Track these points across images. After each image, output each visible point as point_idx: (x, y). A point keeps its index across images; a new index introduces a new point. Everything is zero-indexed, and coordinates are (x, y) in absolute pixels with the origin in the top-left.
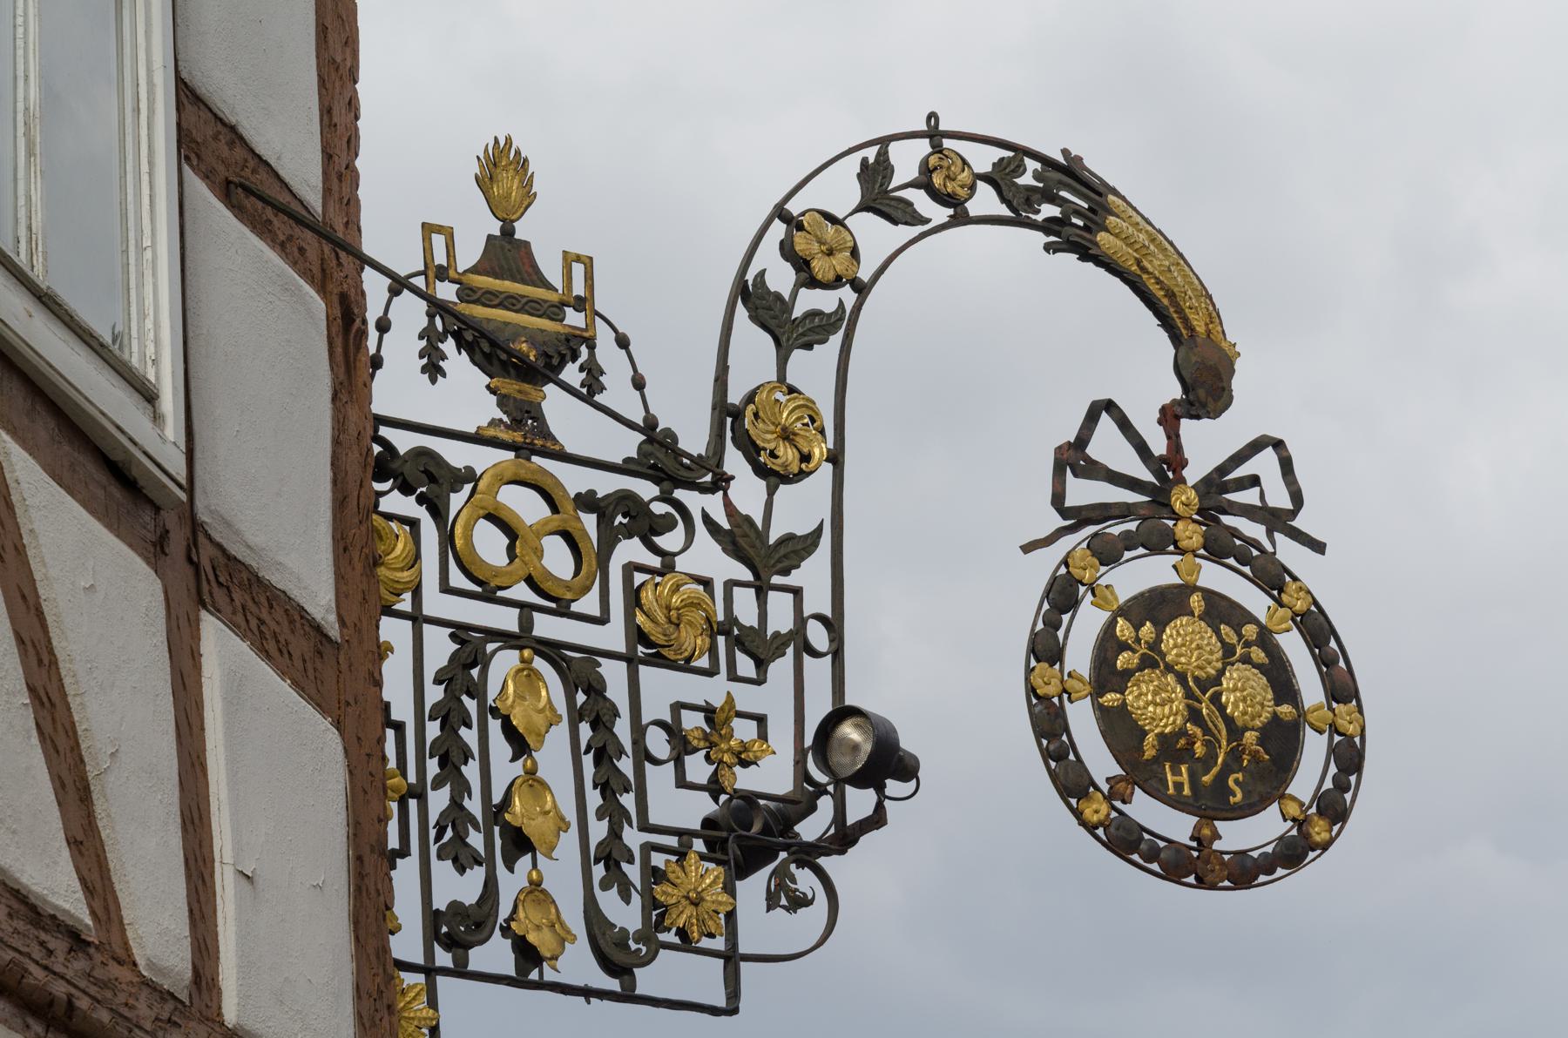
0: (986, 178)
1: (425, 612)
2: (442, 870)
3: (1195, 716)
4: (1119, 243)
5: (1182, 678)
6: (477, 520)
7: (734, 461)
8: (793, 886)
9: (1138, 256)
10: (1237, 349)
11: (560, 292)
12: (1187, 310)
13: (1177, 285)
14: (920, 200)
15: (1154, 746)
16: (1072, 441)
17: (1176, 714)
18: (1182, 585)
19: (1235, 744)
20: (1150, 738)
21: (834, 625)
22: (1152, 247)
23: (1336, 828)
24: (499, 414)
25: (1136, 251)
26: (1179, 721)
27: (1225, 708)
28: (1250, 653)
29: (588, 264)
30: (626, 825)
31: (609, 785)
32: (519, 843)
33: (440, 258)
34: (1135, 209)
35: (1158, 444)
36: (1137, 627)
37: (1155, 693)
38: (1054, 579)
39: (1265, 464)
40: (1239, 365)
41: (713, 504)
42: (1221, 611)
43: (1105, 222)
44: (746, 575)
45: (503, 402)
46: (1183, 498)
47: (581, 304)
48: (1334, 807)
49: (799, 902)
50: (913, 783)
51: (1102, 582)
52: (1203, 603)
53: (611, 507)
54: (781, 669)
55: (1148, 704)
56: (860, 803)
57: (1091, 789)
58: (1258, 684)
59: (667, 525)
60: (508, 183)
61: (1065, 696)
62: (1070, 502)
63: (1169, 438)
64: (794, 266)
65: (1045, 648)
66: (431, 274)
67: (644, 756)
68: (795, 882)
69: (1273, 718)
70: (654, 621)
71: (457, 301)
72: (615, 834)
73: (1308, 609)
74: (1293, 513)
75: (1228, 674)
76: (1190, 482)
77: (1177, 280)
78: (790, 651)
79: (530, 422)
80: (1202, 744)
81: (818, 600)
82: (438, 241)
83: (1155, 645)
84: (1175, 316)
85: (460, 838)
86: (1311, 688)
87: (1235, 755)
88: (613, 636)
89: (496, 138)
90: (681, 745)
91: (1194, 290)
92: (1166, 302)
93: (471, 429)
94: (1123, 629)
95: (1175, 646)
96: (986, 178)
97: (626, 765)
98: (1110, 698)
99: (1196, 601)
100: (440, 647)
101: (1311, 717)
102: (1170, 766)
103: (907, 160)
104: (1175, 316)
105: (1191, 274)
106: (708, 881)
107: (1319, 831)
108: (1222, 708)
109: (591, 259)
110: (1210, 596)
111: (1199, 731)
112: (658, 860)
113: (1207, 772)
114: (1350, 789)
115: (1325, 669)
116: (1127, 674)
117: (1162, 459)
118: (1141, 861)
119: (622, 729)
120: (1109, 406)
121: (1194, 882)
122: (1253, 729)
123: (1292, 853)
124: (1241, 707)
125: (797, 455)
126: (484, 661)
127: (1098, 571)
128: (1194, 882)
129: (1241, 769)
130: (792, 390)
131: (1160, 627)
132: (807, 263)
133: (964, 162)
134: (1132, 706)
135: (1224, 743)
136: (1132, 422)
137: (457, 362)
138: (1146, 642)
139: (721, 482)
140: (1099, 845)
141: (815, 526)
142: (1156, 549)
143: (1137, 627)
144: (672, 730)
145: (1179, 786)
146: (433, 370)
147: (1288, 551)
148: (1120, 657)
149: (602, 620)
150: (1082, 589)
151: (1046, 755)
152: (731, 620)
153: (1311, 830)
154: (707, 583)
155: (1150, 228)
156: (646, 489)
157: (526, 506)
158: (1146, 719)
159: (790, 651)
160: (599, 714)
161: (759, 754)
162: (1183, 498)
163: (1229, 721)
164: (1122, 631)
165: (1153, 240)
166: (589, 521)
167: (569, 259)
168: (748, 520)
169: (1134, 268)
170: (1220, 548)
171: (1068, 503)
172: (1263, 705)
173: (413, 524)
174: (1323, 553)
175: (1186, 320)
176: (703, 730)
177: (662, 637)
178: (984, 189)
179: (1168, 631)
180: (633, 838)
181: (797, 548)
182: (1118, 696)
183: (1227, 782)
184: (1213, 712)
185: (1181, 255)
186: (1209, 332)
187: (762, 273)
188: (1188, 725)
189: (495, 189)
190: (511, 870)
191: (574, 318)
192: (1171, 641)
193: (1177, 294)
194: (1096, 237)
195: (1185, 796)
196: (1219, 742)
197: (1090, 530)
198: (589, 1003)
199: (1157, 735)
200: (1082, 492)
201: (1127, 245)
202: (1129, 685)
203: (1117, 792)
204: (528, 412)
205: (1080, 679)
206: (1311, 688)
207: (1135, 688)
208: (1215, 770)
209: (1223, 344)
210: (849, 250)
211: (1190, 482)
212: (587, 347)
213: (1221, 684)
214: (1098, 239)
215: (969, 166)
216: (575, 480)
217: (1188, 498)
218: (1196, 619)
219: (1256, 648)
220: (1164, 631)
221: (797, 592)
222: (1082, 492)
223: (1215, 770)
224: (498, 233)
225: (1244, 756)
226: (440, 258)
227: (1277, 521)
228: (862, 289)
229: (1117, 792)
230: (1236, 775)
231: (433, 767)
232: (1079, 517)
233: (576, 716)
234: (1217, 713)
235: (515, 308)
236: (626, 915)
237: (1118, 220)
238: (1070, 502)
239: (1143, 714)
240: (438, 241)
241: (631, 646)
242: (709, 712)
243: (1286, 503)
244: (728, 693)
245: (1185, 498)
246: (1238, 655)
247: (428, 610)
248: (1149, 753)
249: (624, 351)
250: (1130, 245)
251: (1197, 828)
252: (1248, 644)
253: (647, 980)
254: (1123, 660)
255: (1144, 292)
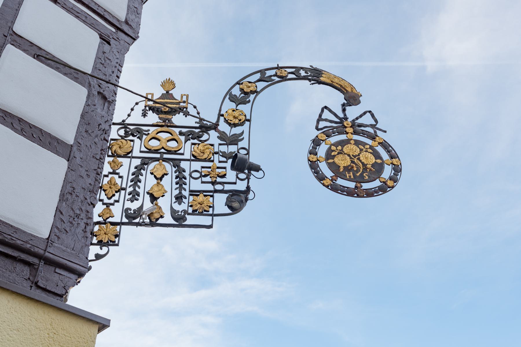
3: (353, 162)
5: (349, 155)
18: (348, 139)
19: (364, 167)
57: (326, 178)
77: (342, 83)
83: (342, 150)
86: (385, 156)
89: (167, 79)
92: (340, 87)
98: (331, 161)
101: (386, 162)
104: (342, 89)
108: (360, 161)
110: (355, 140)
111: (354, 165)
115: (389, 153)
116: (334, 156)
120: (326, 107)
121: (356, 196)
131: (343, 147)
136: (332, 110)
137: (150, 113)
140: (329, 190)
145: (350, 176)
163: (363, 163)
174: (386, 132)
175: (345, 89)
205: (322, 157)
223: (360, 173)
248: (341, 170)
255: (334, 86)
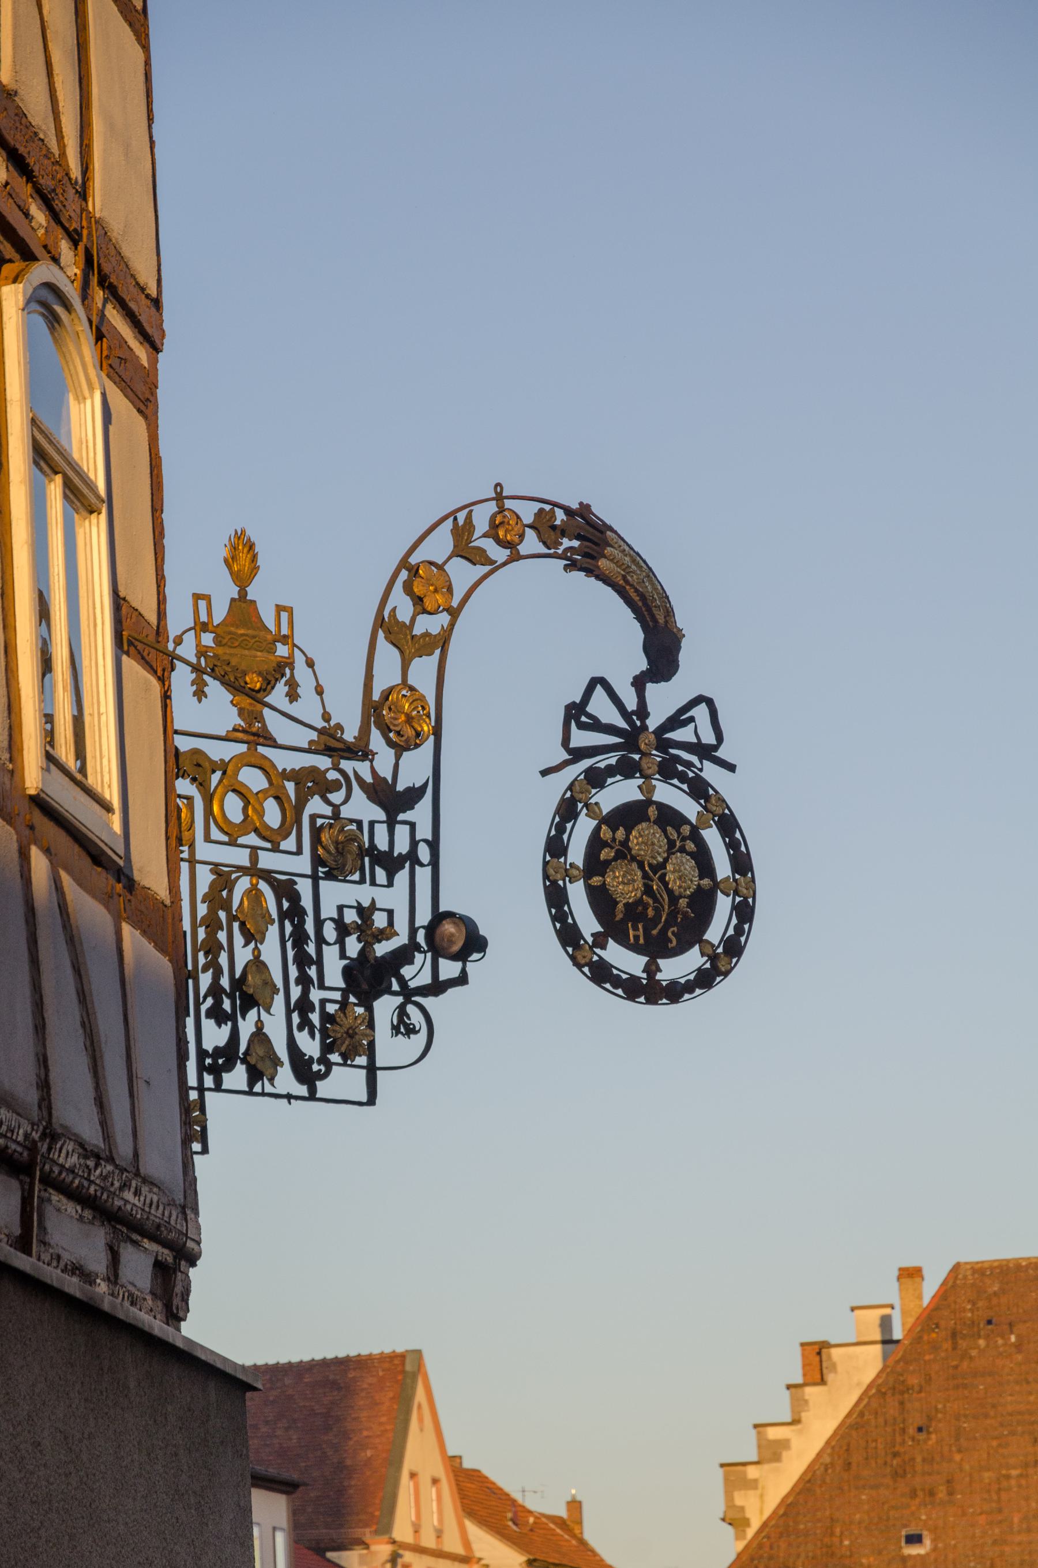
0: (530, 526)
1: (197, 858)
2: (208, 1025)
3: (648, 890)
4: (612, 565)
5: (641, 865)
6: (228, 792)
7: (376, 741)
8: (408, 1022)
9: (622, 572)
10: (683, 632)
11: (274, 633)
12: (653, 609)
13: (648, 592)
14: (489, 546)
15: (622, 912)
16: (578, 702)
17: (637, 890)
19: (673, 908)
20: (620, 906)
21: (434, 845)
22: (633, 567)
23: (734, 960)
24: (239, 722)
25: (623, 570)
26: (639, 895)
27: (668, 884)
28: (685, 845)
29: (290, 610)
30: (312, 988)
31: (303, 960)
32: (249, 1002)
33: (204, 618)
34: (622, 539)
35: (631, 703)
36: (614, 830)
37: (624, 876)
38: (563, 800)
39: (700, 712)
40: (684, 643)
41: (363, 769)
42: (669, 817)
43: (604, 551)
44: (381, 815)
45: (241, 713)
46: (647, 741)
47: (285, 639)
48: (734, 947)
49: (411, 1031)
50: (483, 954)
51: (592, 801)
52: (656, 813)
53: (304, 779)
54: (402, 877)
55: (619, 883)
56: (449, 969)
58: (689, 865)
59: (335, 786)
60: (244, 558)
61: (567, 879)
62: (573, 744)
63: (638, 697)
64: (412, 600)
65: (556, 847)
66: (198, 628)
67: (321, 941)
68: (409, 1018)
69: (697, 888)
70: (328, 851)
71: (214, 646)
72: (305, 993)
73: (723, 813)
74: (716, 748)
75: (670, 861)
76: (651, 729)
78: (407, 865)
79: (257, 724)
80: (653, 909)
81: (424, 832)
82: (202, 604)
83: (625, 843)
84: (646, 613)
85: (218, 1003)
86: (723, 868)
87: (673, 914)
88: (303, 864)
90: (343, 930)
91: (657, 593)
93: (223, 734)
94: (606, 833)
95: (638, 844)
96: (530, 526)
97: (311, 949)
98: (596, 880)
99: (652, 812)
100: (205, 878)
102: (632, 925)
103: (481, 521)
104: (646, 613)
105: (656, 582)
106: (359, 1022)
107: (722, 966)
108: (666, 884)
109: (292, 608)
110: (662, 807)
111: (651, 901)
112: (331, 1008)
113: (655, 928)
114: (744, 934)
116: (607, 863)
117: (633, 713)
118: (611, 989)
119: (310, 926)
120: (602, 681)
121: (547, 860)
122: (685, 897)
123: (705, 980)
124: (678, 884)
125: (414, 733)
126: (230, 885)
127: (590, 793)
128: (547, 860)
129: (676, 924)
130: (412, 689)
132: (421, 599)
133: (518, 517)
134: (609, 885)
135: (666, 907)
137: (213, 687)
138: (620, 841)
139: (366, 755)
141: (424, 781)
142: (628, 775)
143: (614, 830)
144: (340, 925)
146: (200, 694)
147: (711, 772)
148: (603, 852)
149: (299, 852)
150: (580, 805)
151: (554, 919)
152: (373, 845)
153: (719, 964)
154: (359, 823)
155: (632, 552)
156: (323, 762)
157: (253, 779)
158: (617, 894)
159: (407, 865)
160: (294, 913)
161: (389, 935)
162: (647, 741)
163: (670, 892)
164: (604, 834)
165: (634, 561)
166: (290, 787)
167: (280, 609)
168: (385, 779)
169: (621, 582)
170: (668, 771)
171: (572, 745)
172: (692, 881)
173: (190, 799)
176: (357, 923)
177: (334, 863)
178: (530, 534)
179: (634, 834)
180: (316, 995)
181: (414, 795)
182: (601, 878)
183: (667, 933)
184: (660, 887)
185: (650, 569)
186: (666, 622)
187: (394, 609)
188: (644, 897)
189: (235, 566)
190: (244, 1019)
191: (282, 650)
192: (635, 841)
193: (648, 597)
194: (598, 562)
195: (641, 945)
196: (663, 907)
197: (586, 763)
198: (290, 1103)
199: (624, 904)
200: (581, 738)
201: (617, 566)
202: (608, 870)
203: (600, 940)
204: (256, 718)
205: (577, 868)
206: (723, 868)
207: (611, 873)
208: (660, 927)
209: (675, 630)
210: (446, 588)
211: (651, 729)
212: (289, 669)
213: (666, 868)
214: (600, 564)
215: (521, 520)
216: (285, 761)
217: (649, 741)
218: (652, 824)
219: (688, 841)
220: (631, 833)
221: (412, 826)
222: (581, 738)
223: (660, 927)
224: (237, 597)
225: (679, 916)
226: (204, 618)
227: (706, 752)
228: (454, 613)
229: (600, 940)
230: (672, 929)
231: (202, 960)
232: (577, 754)
233: (283, 915)
234: (662, 887)
235: (247, 647)
236: (310, 1046)
237: (612, 549)
238: (573, 744)
239: (615, 891)
240: (202, 604)
241: (315, 870)
242: (360, 909)
243: (713, 741)
244: (373, 898)
245: (646, 741)
246: (677, 847)
247: (199, 856)
248: (619, 916)
249: (310, 669)
250: (619, 567)
251: (647, 965)
252: (684, 839)
253: (323, 1088)
254: (605, 854)
